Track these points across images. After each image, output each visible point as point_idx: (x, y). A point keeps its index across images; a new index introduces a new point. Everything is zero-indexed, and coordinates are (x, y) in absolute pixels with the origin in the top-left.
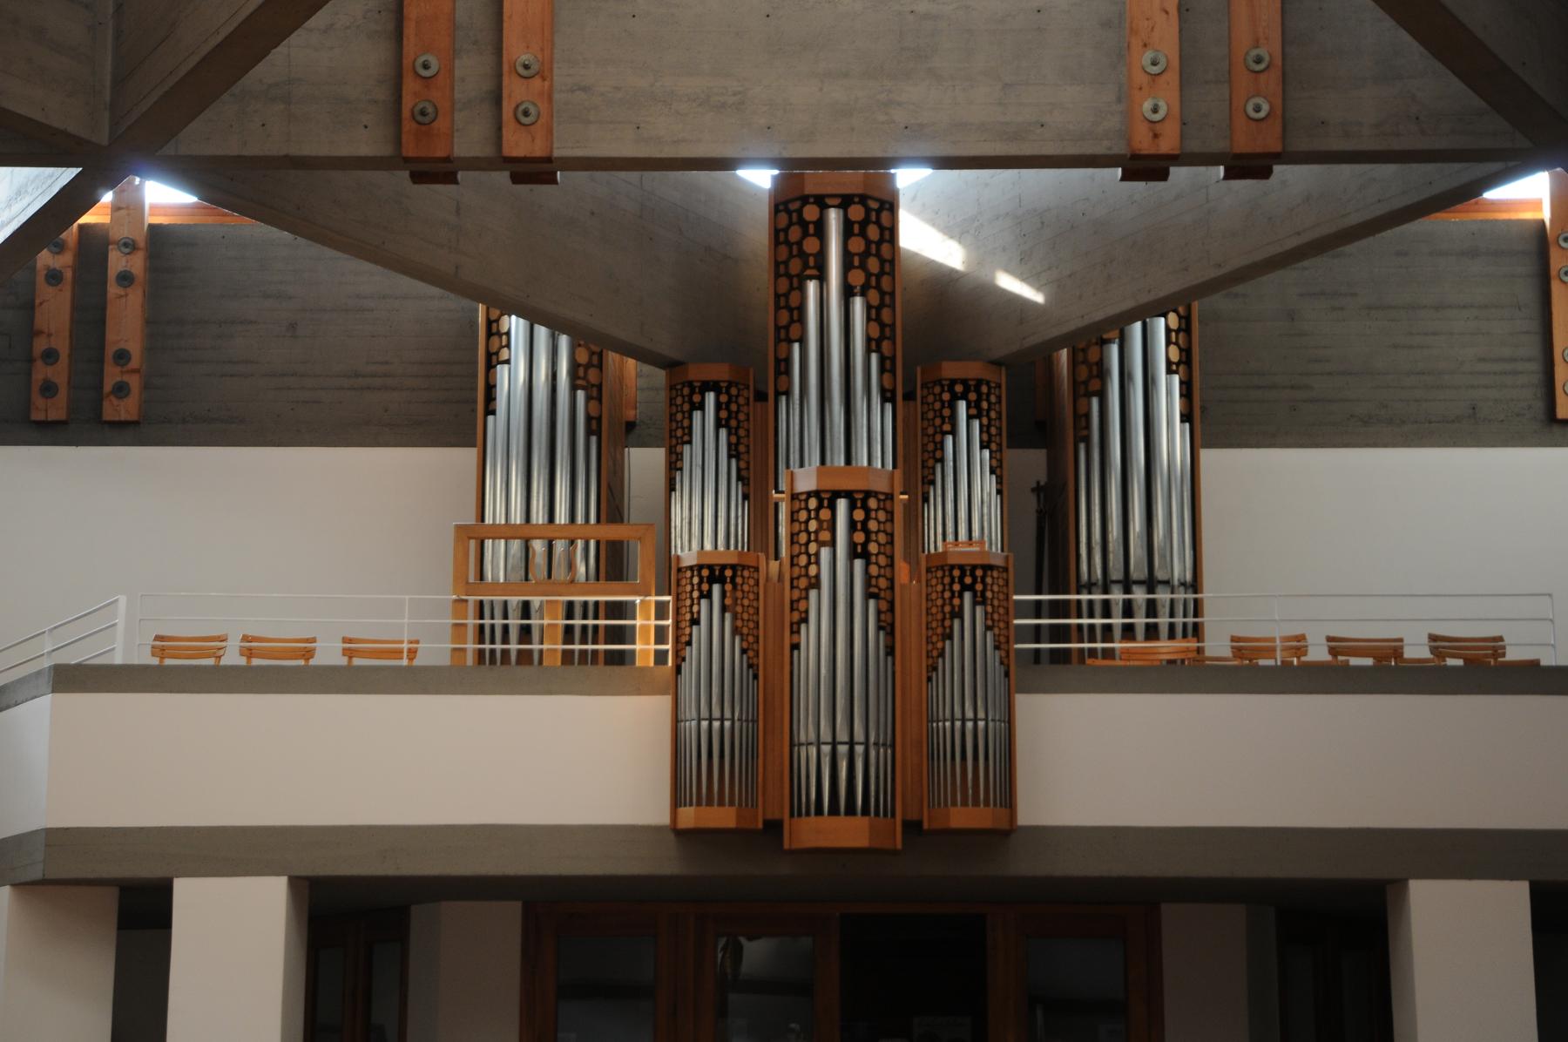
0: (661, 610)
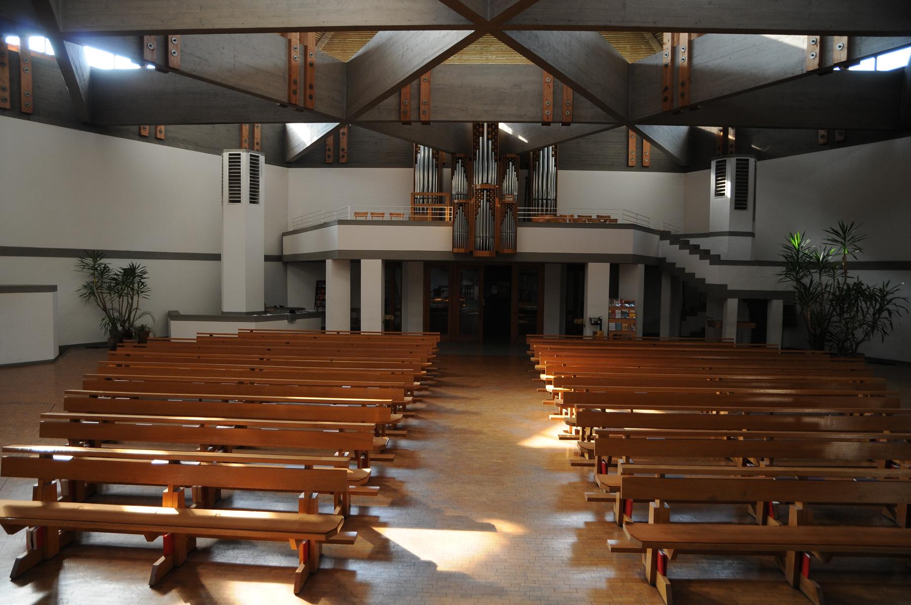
0: (450, 210)
